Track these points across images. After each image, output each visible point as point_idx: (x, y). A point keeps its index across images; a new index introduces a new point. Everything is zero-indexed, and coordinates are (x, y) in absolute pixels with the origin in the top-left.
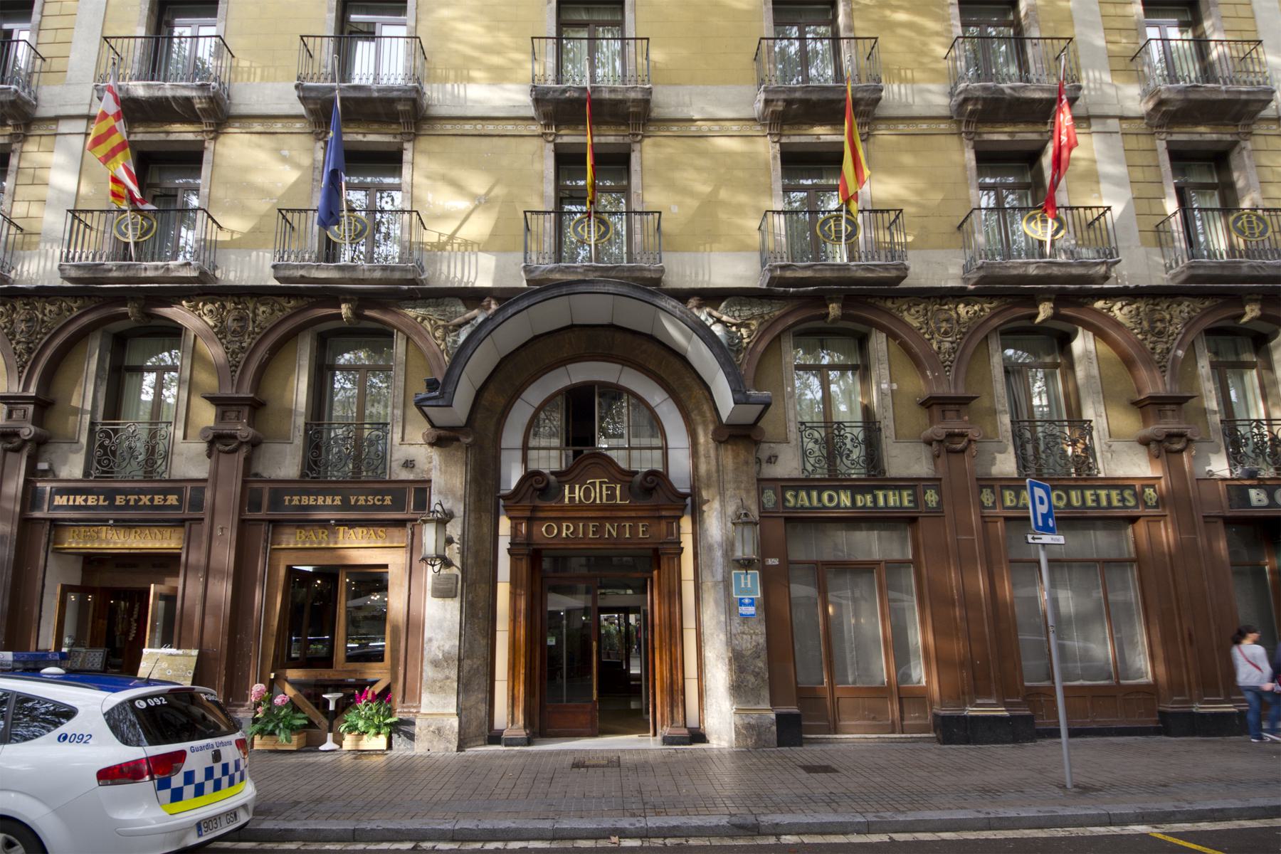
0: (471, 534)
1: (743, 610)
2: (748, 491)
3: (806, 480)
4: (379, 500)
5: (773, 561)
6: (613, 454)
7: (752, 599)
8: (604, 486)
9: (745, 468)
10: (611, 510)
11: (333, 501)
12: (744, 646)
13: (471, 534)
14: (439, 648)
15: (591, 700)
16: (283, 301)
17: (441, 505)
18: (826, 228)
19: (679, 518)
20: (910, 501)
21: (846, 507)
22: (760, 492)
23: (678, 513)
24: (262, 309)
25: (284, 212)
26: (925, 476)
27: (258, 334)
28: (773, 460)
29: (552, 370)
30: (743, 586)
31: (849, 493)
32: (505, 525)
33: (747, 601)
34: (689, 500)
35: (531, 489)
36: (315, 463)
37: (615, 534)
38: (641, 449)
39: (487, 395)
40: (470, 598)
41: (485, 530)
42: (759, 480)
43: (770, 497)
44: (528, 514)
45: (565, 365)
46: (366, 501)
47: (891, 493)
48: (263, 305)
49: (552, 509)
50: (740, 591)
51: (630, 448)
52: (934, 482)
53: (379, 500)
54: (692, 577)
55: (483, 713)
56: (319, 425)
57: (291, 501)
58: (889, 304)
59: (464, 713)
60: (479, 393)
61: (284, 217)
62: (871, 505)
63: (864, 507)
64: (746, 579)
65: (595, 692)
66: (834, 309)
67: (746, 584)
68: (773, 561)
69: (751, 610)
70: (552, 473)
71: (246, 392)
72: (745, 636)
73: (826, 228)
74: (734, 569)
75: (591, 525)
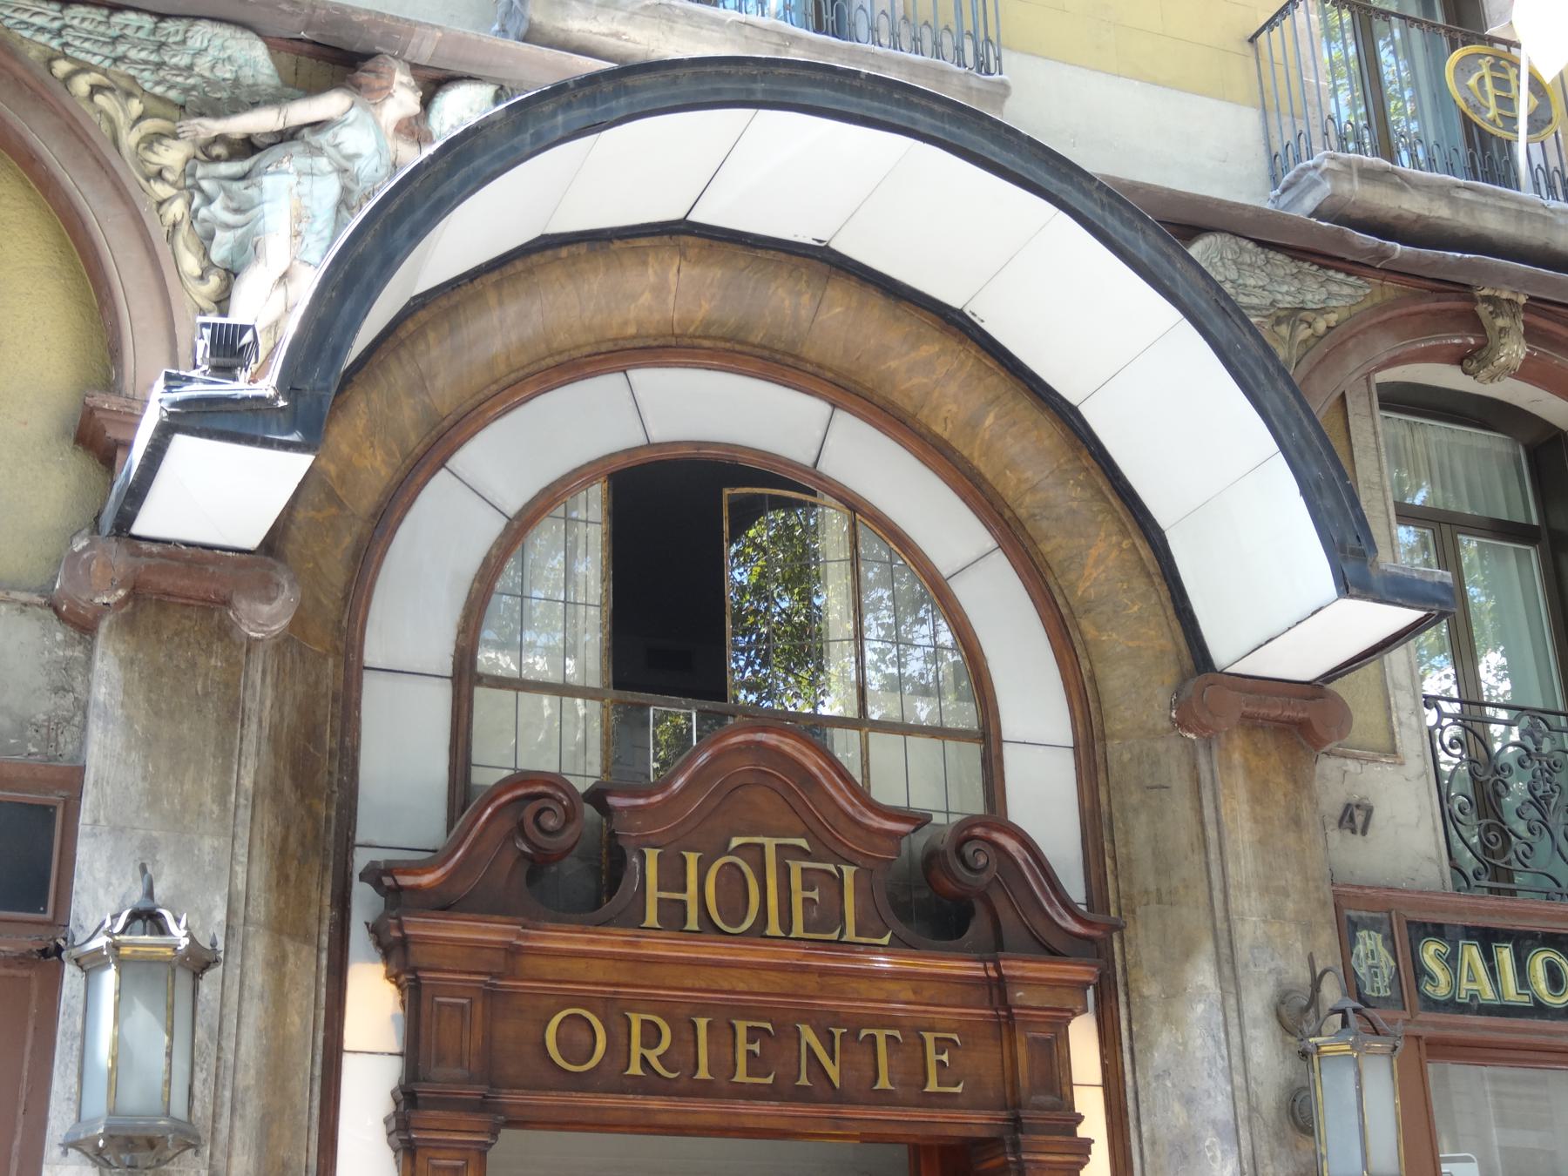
8: (796, 867)
9: (1291, 839)
18: (1472, 82)
22: (1347, 932)
28: (1359, 818)
29: (602, 374)
37: (833, 1072)
73: (1472, 82)
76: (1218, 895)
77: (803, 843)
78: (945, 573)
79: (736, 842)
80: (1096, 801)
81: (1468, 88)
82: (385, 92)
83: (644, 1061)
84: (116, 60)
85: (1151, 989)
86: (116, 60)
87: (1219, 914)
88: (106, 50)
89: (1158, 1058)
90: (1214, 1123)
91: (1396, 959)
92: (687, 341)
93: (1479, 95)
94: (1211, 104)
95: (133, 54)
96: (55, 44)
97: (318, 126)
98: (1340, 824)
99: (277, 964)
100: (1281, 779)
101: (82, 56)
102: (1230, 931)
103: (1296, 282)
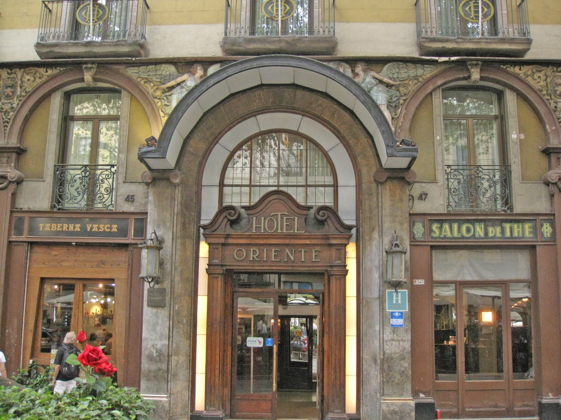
0: (177, 257)
1: (394, 321)
2: (401, 224)
3: (449, 214)
4: (108, 228)
5: (420, 282)
6: (291, 191)
7: (401, 313)
8: (285, 218)
10: (290, 238)
11: (74, 228)
12: (393, 351)
13: (177, 257)
14: (153, 346)
15: (272, 391)
16: (42, 70)
17: (155, 233)
18: (467, 9)
19: (345, 245)
20: (530, 232)
21: (480, 238)
22: (412, 225)
23: (344, 242)
24: (27, 77)
25: (46, 3)
26: (544, 212)
27: (24, 96)
28: (423, 197)
30: (394, 302)
31: (483, 226)
32: (204, 249)
33: (397, 314)
34: (354, 231)
35: (226, 220)
36: (60, 196)
37: (292, 258)
38: (316, 186)
39: (192, 143)
40: (177, 308)
41: (189, 253)
42: (410, 215)
43: (419, 229)
44: (222, 241)
45: (255, 116)
46: (99, 228)
47: (515, 226)
48: (27, 74)
49: (241, 237)
50: (392, 306)
51: (307, 186)
52: (551, 218)
53: (108, 228)
54: (355, 294)
55: (187, 398)
56: (62, 166)
57: (44, 227)
58: (517, 69)
59: (172, 397)
60: (186, 141)
61: (46, 6)
62: (500, 235)
63: (494, 237)
64: (397, 296)
65: (275, 385)
66: (476, 75)
67: (397, 300)
68: (420, 282)
69: (400, 321)
70: (243, 207)
71: (13, 142)
72: (394, 343)
73: (467, 9)
74: (388, 288)
75: (273, 250)
76: (380, 218)
77: (286, 213)
78: (327, 150)
79: (272, 214)
80: (359, 198)
81: (466, 10)
82: (196, 71)
83: (253, 257)
84: (149, 76)
85: (367, 238)
86: (149, 76)
87: (380, 222)
88: (146, 74)
89: (367, 252)
90: (375, 266)
91: (424, 229)
92: (268, 108)
93: (469, 12)
94: (402, 25)
95: (151, 74)
96: (138, 75)
97: (184, 81)
98: (419, 199)
99: (183, 244)
100: (399, 191)
101: (143, 76)
102: (382, 226)
103: (415, 70)
